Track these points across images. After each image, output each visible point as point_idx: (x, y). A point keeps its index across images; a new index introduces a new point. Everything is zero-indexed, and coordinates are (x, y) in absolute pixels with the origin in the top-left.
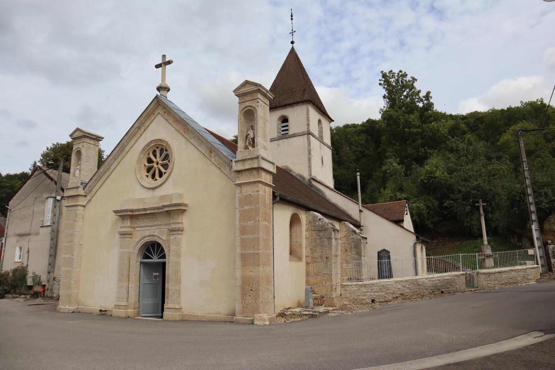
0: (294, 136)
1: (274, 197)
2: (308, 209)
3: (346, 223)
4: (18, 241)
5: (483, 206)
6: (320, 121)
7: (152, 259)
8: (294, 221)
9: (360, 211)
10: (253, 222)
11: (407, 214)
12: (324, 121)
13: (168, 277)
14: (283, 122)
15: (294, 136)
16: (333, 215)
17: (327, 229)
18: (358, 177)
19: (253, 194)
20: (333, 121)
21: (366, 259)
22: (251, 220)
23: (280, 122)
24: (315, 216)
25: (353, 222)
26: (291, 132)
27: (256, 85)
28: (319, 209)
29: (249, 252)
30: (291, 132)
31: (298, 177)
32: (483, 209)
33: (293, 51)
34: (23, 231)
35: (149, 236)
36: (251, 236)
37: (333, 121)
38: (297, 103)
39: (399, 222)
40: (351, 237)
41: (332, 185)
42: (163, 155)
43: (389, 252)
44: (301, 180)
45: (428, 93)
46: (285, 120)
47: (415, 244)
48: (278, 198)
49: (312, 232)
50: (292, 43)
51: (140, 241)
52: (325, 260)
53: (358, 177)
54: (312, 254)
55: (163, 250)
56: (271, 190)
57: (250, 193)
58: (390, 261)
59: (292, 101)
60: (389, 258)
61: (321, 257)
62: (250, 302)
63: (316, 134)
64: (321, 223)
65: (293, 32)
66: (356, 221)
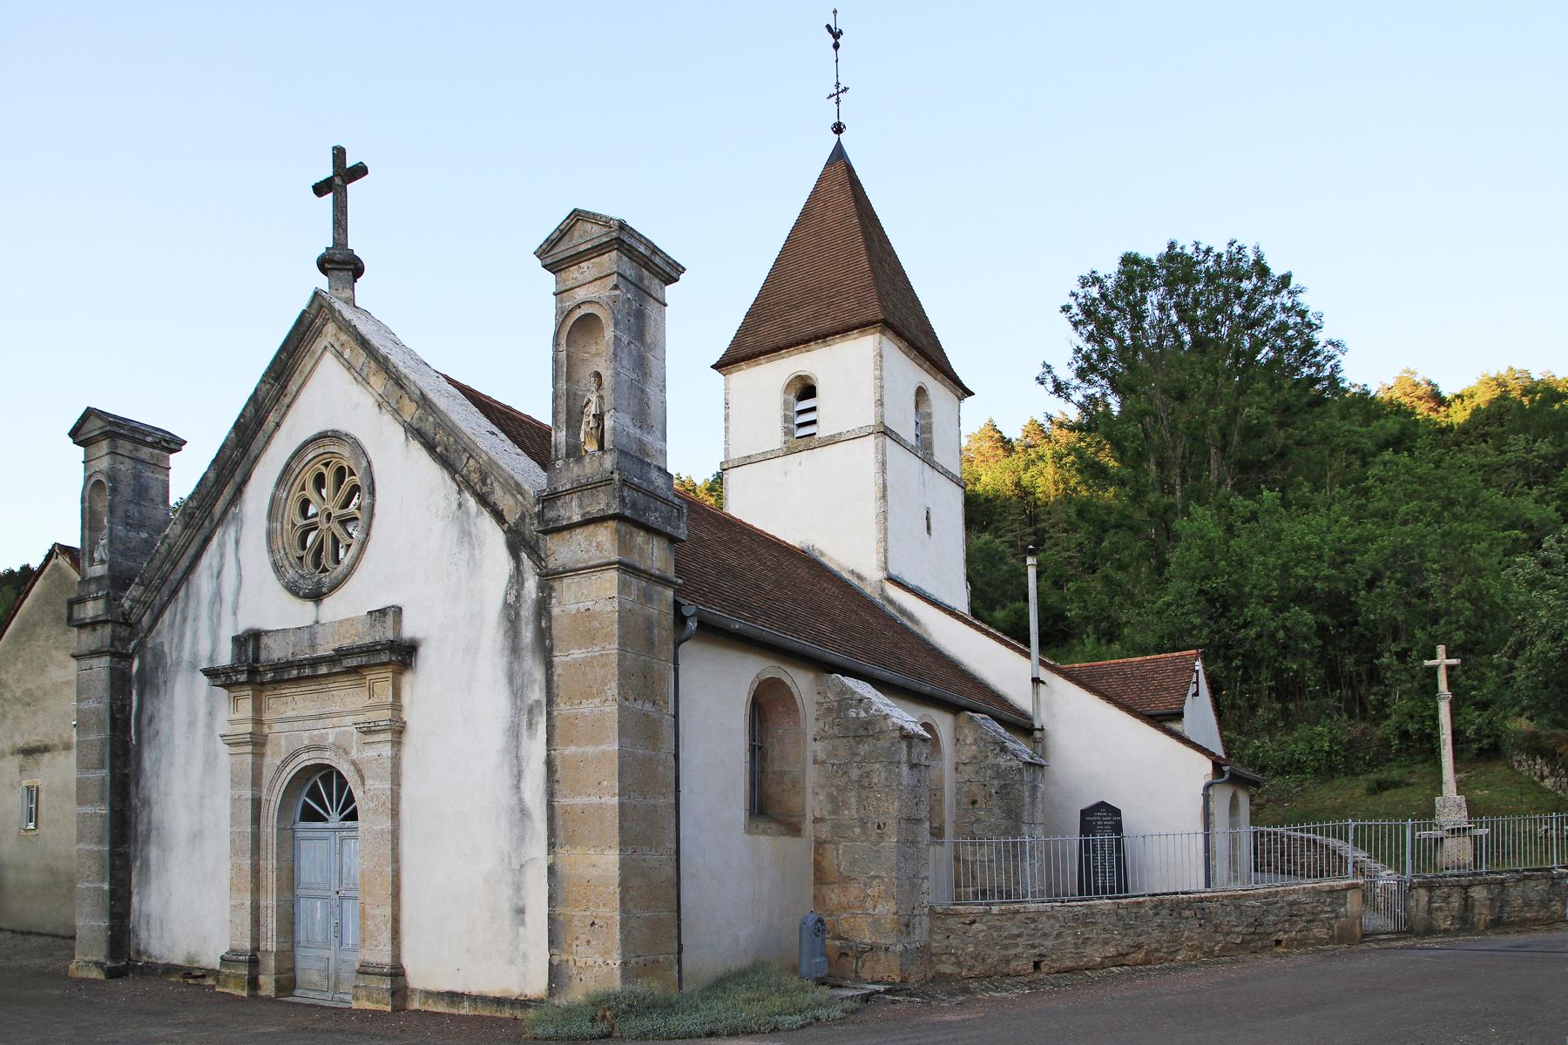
0: (833, 440)
1: (680, 620)
2: (824, 667)
3: (978, 716)
4: (22, 769)
5: (1450, 668)
6: (921, 392)
7: (325, 820)
8: (766, 706)
9: (1036, 681)
10: (597, 701)
11: (1196, 694)
12: (938, 392)
13: (1133, 862)
14: (801, 398)
15: (833, 440)
16: (927, 688)
17: (881, 732)
18: (1032, 573)
19: (598, 607)
20: (971, 394)
21: (1039, 831)
22: (588, 696)
23: (792, 398)
24: (845, 690)
25: (1006, 715)
26: (822, 431)
27: (606, 222)
28: (867, 666)
29: (585, 800)
30: (822, 431)
31: (846, 575)
32: (1448, 677)
33: (839, 154)
34: (33, 740)
35: (308, 749)
36: (591, 749)
37: (971, 394)
38: (844, 331)
39: (1164, 719)
40: (991, 760)
41: (962, 603)
42: (345, 488)
43: (1117, 812)
44: (855, 581)
45: (1257, 250)
46: (806, 389)
47: (1208, 787)
48: (692, 625)
49: (838, 741)
50: (838, 128)
51: (285, 763)
52: (874, 833)
53: (1032, 573)
54: (835, 811)
55: (350, 799)
56: (670, 593)
57: (589, 604)
58: (1118, 841)
59: (826, 324)
60: (1117, 828)
61: (863, 823)
62: (590, 961)
63: (909, 434)
64: (863, 714)
65: (839, 92)
66: (1022, 714)
